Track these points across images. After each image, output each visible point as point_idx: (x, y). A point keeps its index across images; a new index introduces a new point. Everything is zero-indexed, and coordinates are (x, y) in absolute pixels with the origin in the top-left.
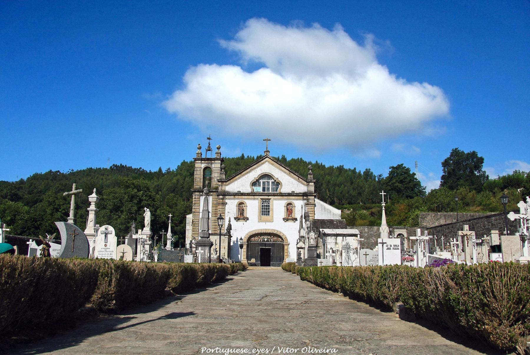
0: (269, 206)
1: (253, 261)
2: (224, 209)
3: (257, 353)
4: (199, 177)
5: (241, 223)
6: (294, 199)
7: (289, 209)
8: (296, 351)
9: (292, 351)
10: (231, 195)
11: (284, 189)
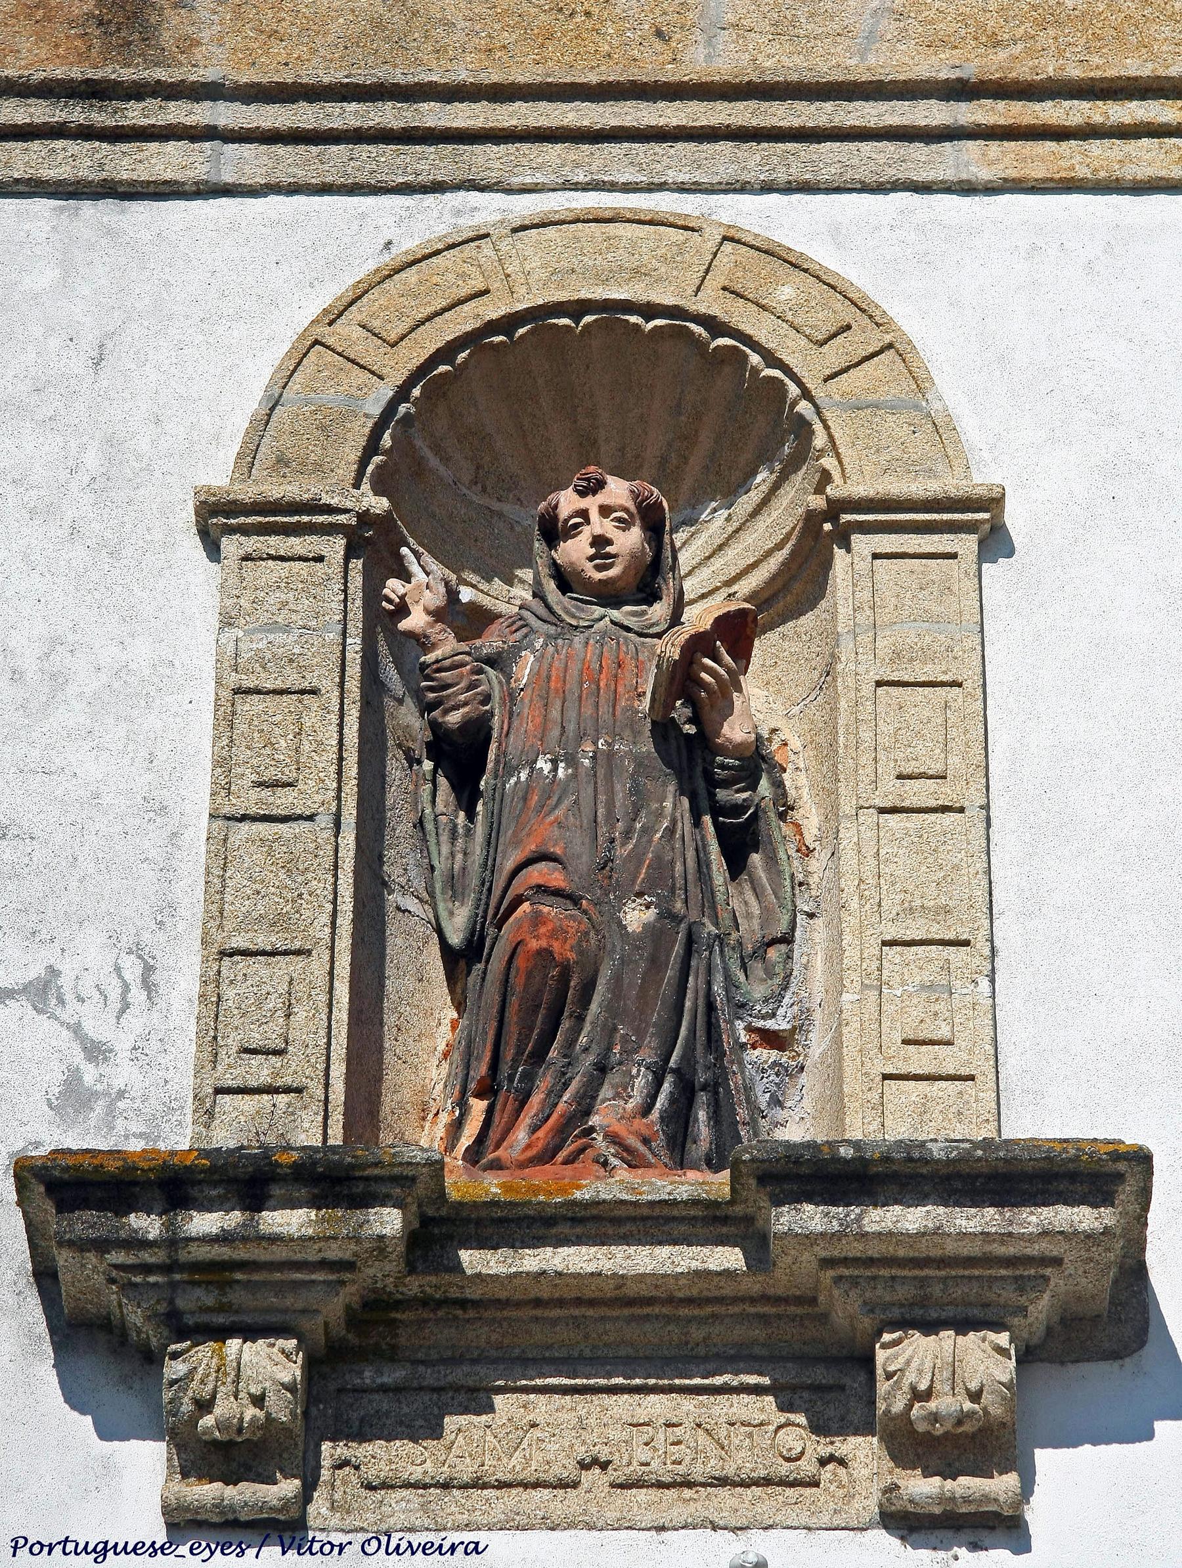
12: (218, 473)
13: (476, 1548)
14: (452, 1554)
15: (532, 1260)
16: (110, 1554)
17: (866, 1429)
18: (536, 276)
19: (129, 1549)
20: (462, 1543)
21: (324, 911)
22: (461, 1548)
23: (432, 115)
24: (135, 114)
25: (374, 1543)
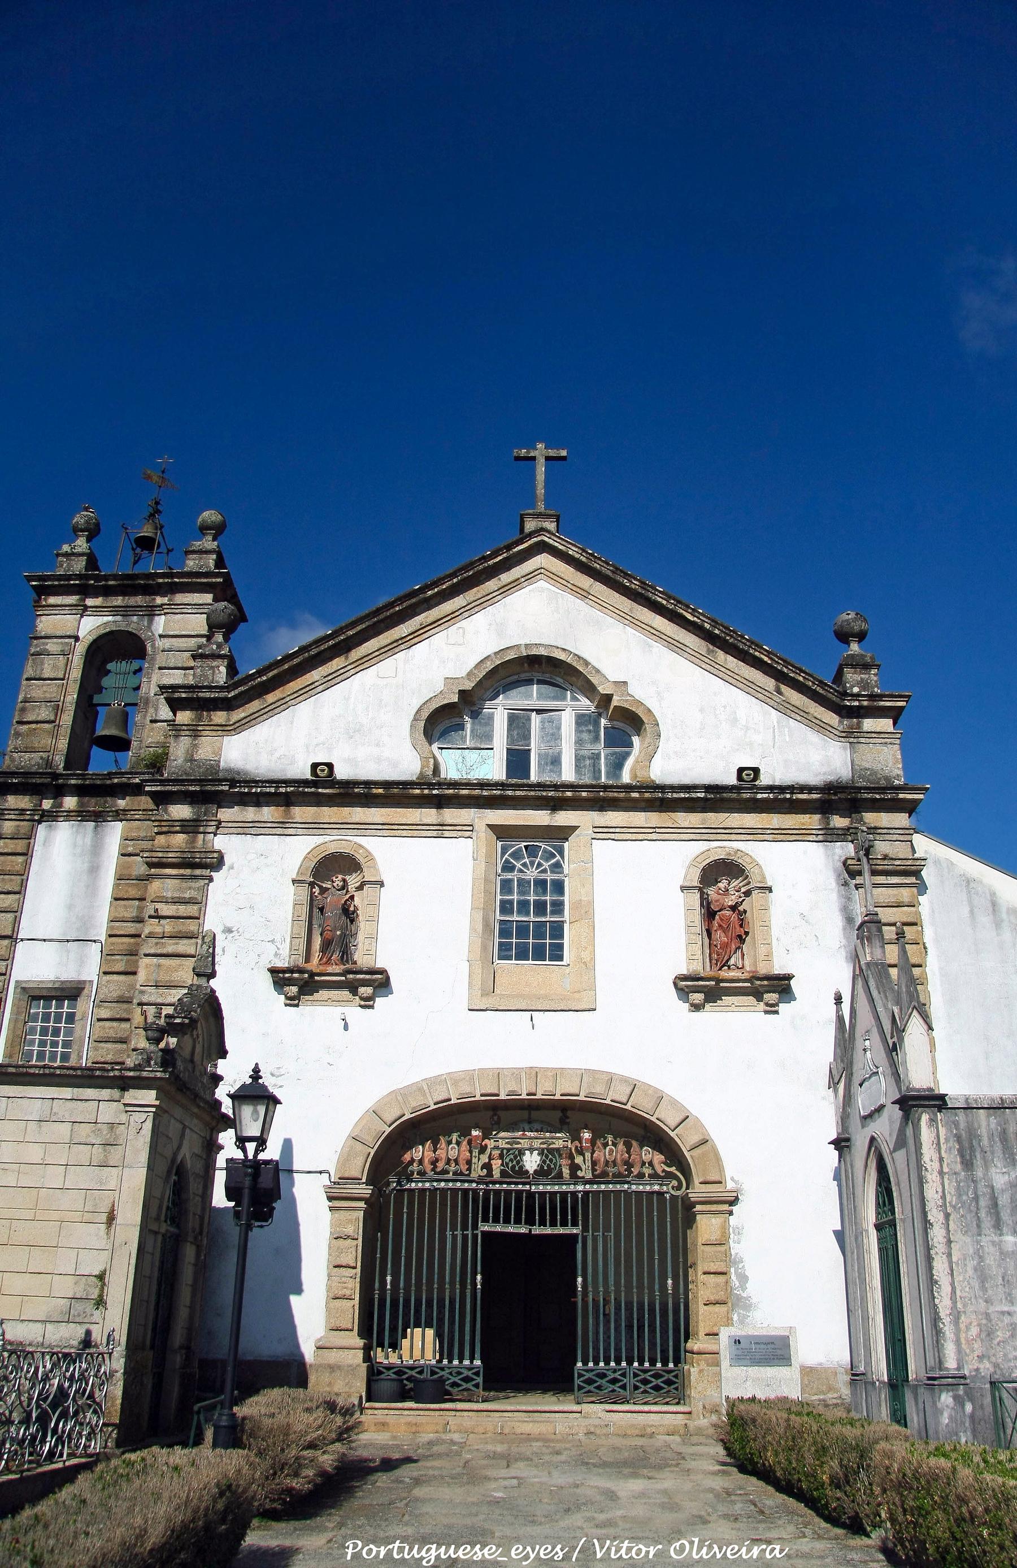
0: (559, 887)
1: (420, 1346)
2: (199, 902)
3: (527, 1557)
4: (51, 690)
5: (324, 1014)
6: (753, 834)
7: (723, 903)
8: (652, 1551)
9: (639, 1551)
10: (258, 800)
11: (676, 758)
12: (294, 877)
18: (332, 849)
21: (303, 932)
23: (322, 826)
24: (287, 825)
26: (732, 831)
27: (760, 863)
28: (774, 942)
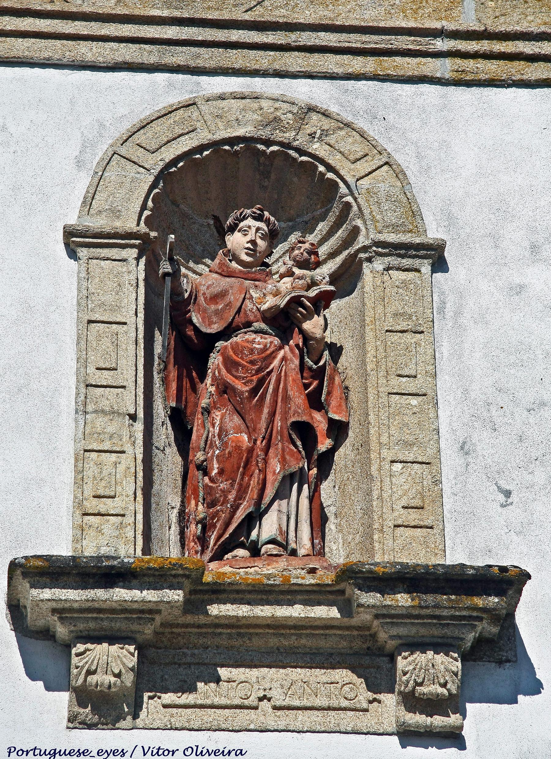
13: (241, 753)
14: (229, 755)
15: (282, 612)
16: (57, 755)
17: (392, 691)
19: (67, 753)
20: (234, 750)
22: (234, 752)
25: (190, 750)
26: (292, 38)
27: (399, 158)
28: (450, 462)
